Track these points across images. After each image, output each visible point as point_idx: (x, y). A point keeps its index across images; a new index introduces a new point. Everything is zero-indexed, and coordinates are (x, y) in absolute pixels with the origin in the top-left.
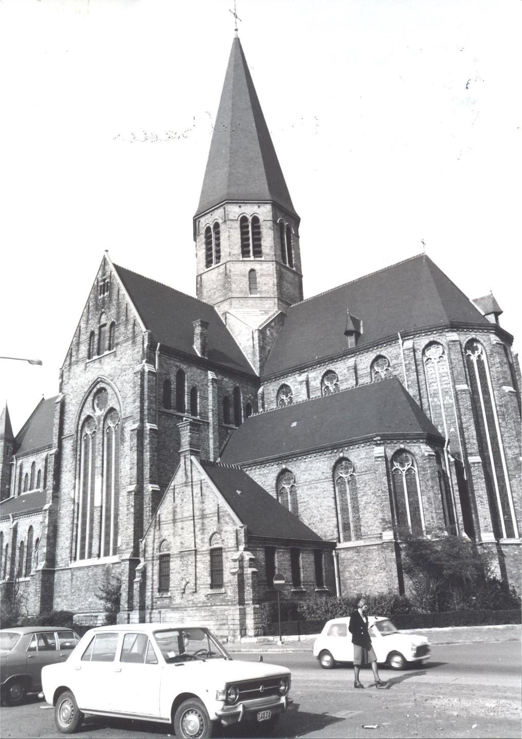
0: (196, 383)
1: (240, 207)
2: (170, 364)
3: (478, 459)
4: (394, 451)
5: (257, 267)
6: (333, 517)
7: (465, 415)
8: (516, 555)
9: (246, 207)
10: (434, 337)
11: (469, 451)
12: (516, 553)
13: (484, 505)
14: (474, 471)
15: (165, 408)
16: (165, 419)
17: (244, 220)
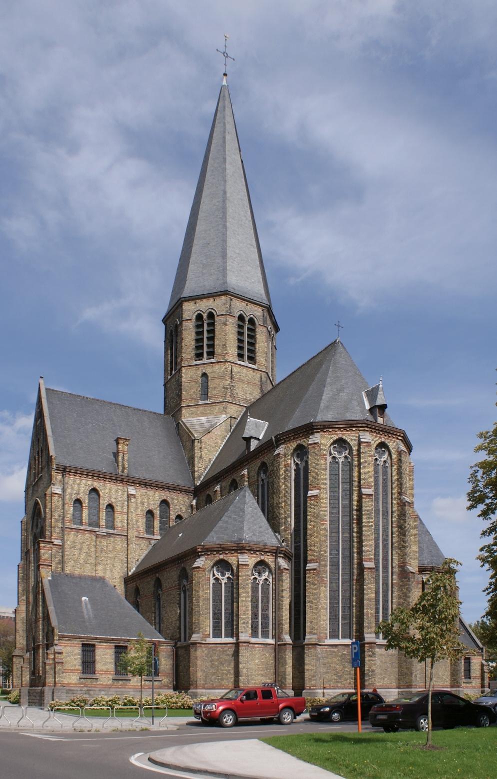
0: (112, 500)
1: (195, 303)
2: (80, 484)
3: (367, 564)
4: (214, 562)
5: (208, 370)
6: (373, 602)
7: (311, 521)
8: (345, 655)
9: (201, 303)
10: (385, 439)
11: (309, 558)
12: (344, 652)
13: (312, 609)
14: (308, 577)
15: (74, 524)
16: (74, 535)
17: (199, 317)
